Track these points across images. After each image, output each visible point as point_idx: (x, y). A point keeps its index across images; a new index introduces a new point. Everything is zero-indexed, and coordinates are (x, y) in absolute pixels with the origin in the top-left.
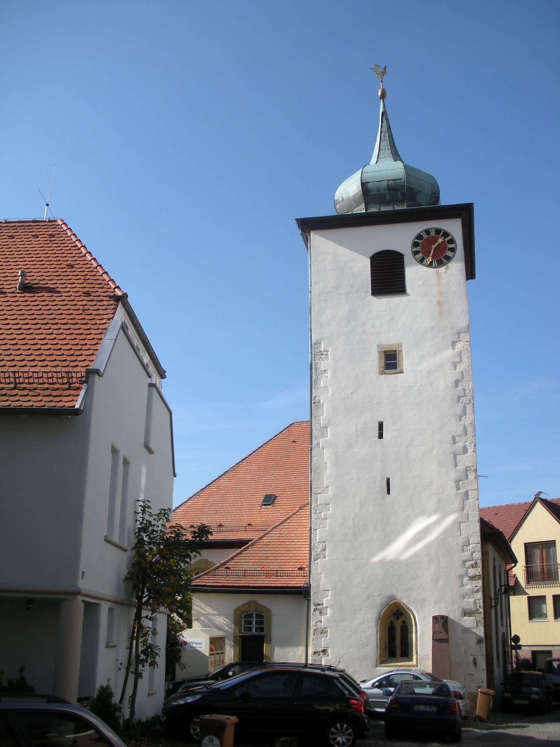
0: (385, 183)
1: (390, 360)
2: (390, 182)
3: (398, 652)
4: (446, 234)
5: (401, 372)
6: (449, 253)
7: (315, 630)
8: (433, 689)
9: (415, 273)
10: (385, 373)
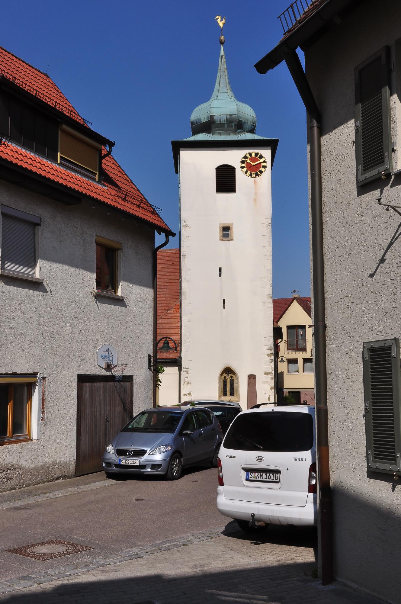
0: (225, 117)
1: (226, 231)
2: (228, 116)
3: (228, 393)
4: (261, 157)
5: (232, 240)
6: (262, 169)
7: (184, 382)
8: (165, 368)
9: (241, 178)
10: (223, 240)
